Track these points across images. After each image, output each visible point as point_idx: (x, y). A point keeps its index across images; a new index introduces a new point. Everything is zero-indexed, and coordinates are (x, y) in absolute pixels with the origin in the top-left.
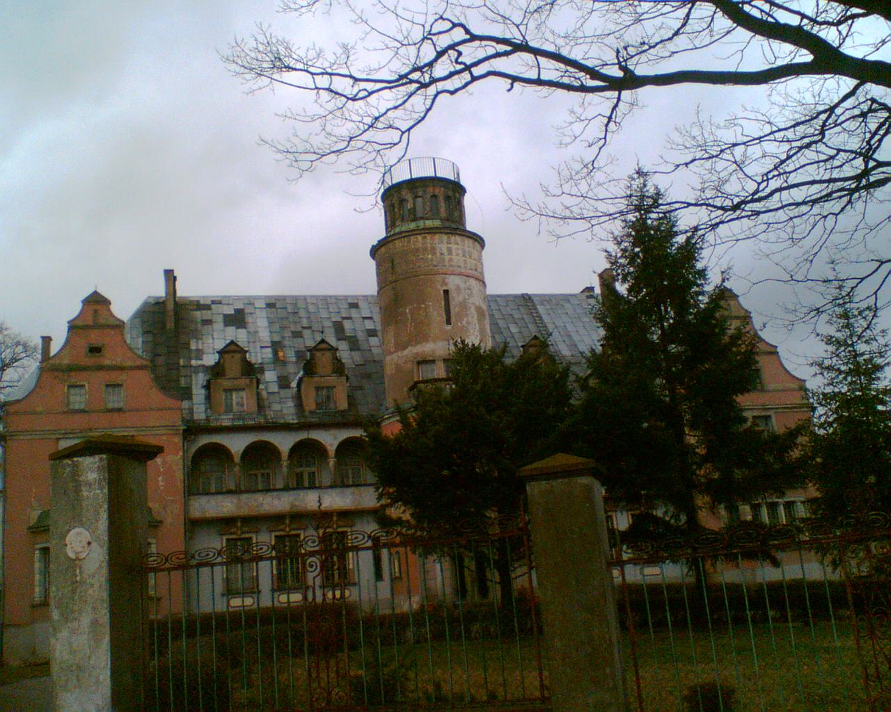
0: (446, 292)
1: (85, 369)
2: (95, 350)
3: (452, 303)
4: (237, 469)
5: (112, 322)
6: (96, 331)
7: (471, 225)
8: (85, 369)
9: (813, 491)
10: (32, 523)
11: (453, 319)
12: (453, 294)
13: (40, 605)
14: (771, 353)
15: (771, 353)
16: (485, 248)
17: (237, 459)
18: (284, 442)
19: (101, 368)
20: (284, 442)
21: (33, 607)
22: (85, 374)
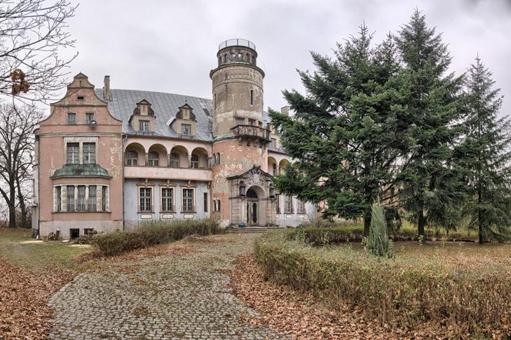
0: (252, 91)
1: (76, 106)
2: (81, 98)
3: (254, 97)
4: (147, 156)
5: (88, 86)
6: (81, 90)
7: (259, 64)
8: (76, 106)
9: (326, 179)
10: (52, 175)
11: (253, 103)
12: (254, 93)
13: (56, 213)
14: (90, 88)
15: (90, 88)
16: (266, 74)
17: (147, 151)
18: (169, 146)
19: (83, 106)
20: (169, 146)
21: (53, 213)
22: (76, 108)
